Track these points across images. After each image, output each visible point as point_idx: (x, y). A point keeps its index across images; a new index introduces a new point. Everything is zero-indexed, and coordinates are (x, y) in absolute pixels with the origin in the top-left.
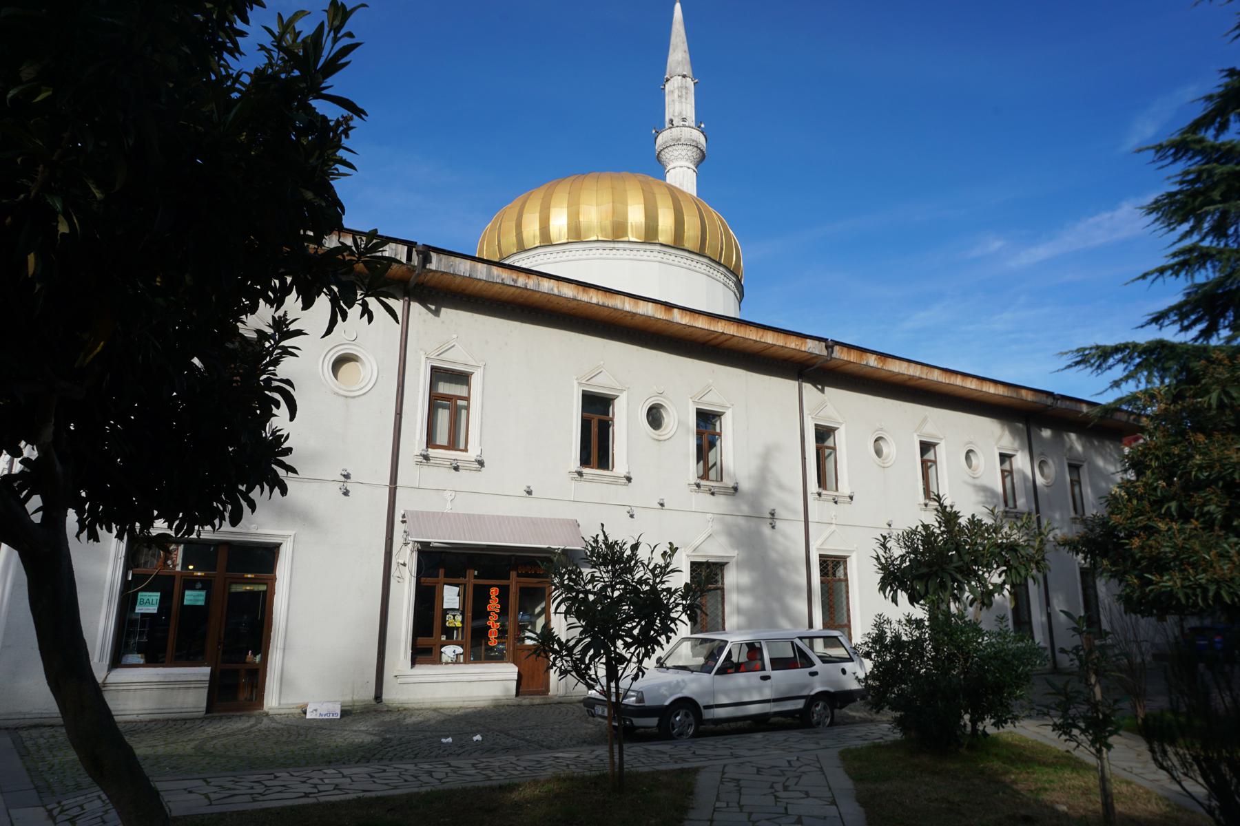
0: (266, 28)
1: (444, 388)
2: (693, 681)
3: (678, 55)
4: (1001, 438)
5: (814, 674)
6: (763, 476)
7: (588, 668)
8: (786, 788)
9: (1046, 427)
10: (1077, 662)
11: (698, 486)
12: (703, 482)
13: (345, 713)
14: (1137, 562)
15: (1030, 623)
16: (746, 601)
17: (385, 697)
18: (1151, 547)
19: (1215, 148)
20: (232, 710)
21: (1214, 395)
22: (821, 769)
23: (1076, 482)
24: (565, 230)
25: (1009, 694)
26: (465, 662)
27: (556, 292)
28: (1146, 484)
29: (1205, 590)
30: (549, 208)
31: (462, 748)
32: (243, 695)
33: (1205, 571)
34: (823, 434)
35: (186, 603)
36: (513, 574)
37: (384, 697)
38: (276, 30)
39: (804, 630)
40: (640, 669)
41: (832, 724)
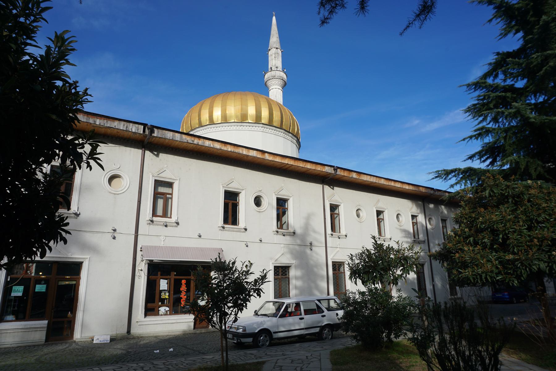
1: (161, 190)
2: (268, 321)
3: (274, 39)
4: (412, 208)
5: (324, 316)
6: (307, 227)
9: (431, 203)
11: (277, 232)
12: (279, 230)
13: (112, 340)
15: (425, 289)
16: (299, 283)
18: (462, 257)
19: (490, 86)
21: (487, 192)
22: (320, 360)
23: (444, 227)
24: (220, 118)
25: (402, 324)
26: (170, 314)
27: (212, 146)
28: (462, 230)
29: (481, 276)
30: (213, 107)
33: (481, 268)
34: (334, 208)
35: (36, 290)
39: (325, 296)
41: (332, 338)
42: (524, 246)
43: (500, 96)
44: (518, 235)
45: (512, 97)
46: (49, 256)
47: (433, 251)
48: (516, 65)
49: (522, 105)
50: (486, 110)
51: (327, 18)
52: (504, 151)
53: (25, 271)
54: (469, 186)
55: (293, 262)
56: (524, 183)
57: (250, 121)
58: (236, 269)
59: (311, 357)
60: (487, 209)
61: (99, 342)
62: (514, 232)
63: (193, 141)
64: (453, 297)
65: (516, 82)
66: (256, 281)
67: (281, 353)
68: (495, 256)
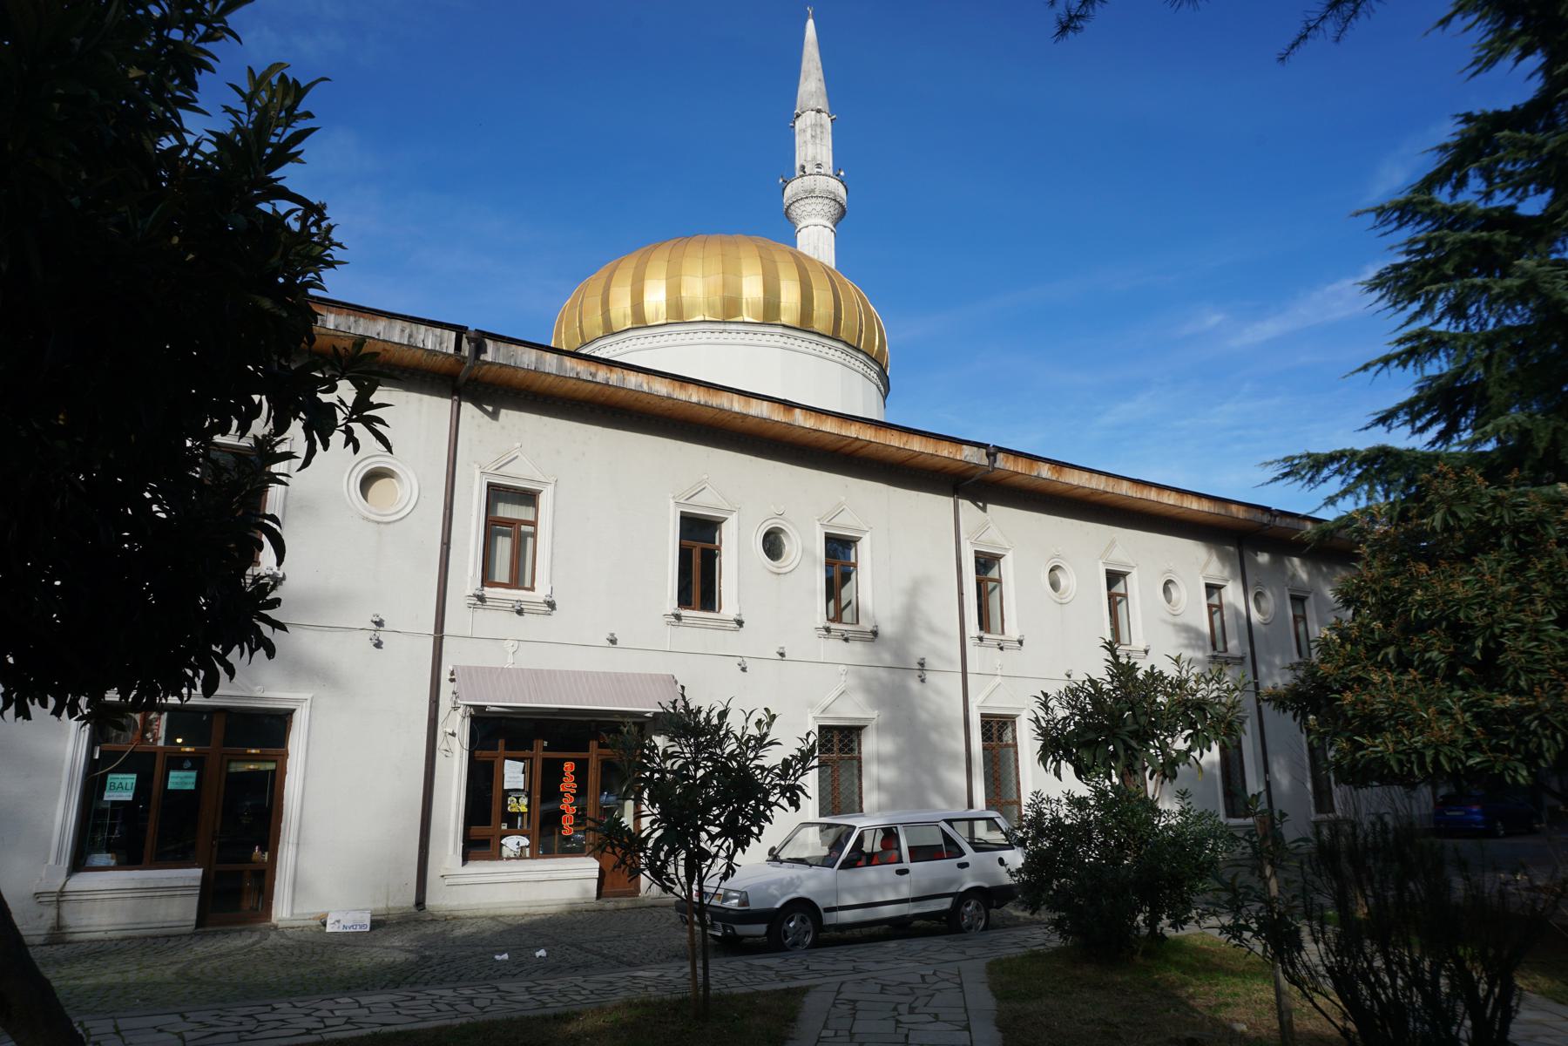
1: (506, 511)
2: (809, 877)
3: (811, 84)
4: (1206, 565)
5: (964, 865)
6: (910, 616)
7: (665, 863)
8: (912, 1010)
9: (1263, 551)
10: (1249, 850)
11: (828, 630)
12: (833, 626)
13: (376, 924)
14: (1348, 721)
16: (888, 774)
17: (428, 902)
18: (1364, 702)
19: (1446, 211)
20: (238, 923)
21: (1438, 516)
23: (1300, 618)
25: (1191, 888)
26: (532, 857)
27: (645, 388)
29: (1421, 756)
30: (642, 280)
31: (521, 967)
32: (247, 903)
33: (1421, 732)
34: (985, 563)
35: (170, 786)
36: (593, 744)
39: (960, 811)
40: (730, 867)
41: (986, 928)
42: (1547, 671)
43: (1475, 240)
44: (1530, 639)
45: (1509, 243)
46: (228, 693)
47: (1267, 685)
48: (1521, 149)
49: (1539, 265)
50: (1433, 281)
51: (1078, 17)
52: (1484, 398)
53: (138, 733)
54: (1382, 500)
55: (873, 714)
56: (1546, 490)
58: (728, 732)
59: (935, 979)
60: (1437, 564)
61: (341, 930)
62: (1519, 630)
63: (594, 375)
64: (1324, 816)
65: (1520, 200)
66: (786, 764)
67: (850, 966)
68: (1461, 699)
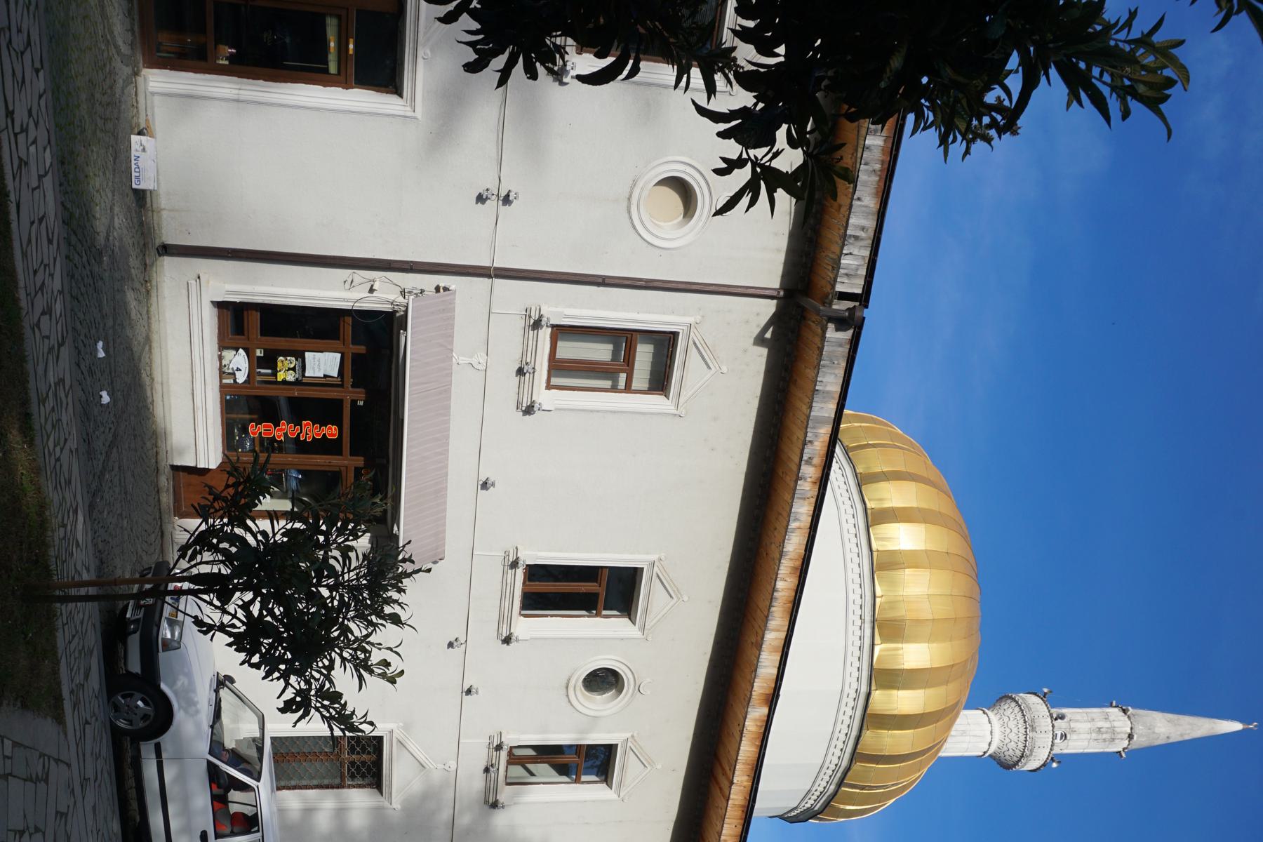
0: (1162, 20)
2: (198, 725)
3: (1164, 727)
7: (215, 549)
11: (499, 748)
12: (504, 755)
13: (141, 197)
16: (323, 822)
24: (890, 546)
26: (222, 386)
27: (793, 525)
32: (165, 38)
36: (359, 461)
37: (166, 258)
38: (1157, 38)
57: (877, 649)
58: (375, 625)
61: (133, 153)
67: (90, 774)
